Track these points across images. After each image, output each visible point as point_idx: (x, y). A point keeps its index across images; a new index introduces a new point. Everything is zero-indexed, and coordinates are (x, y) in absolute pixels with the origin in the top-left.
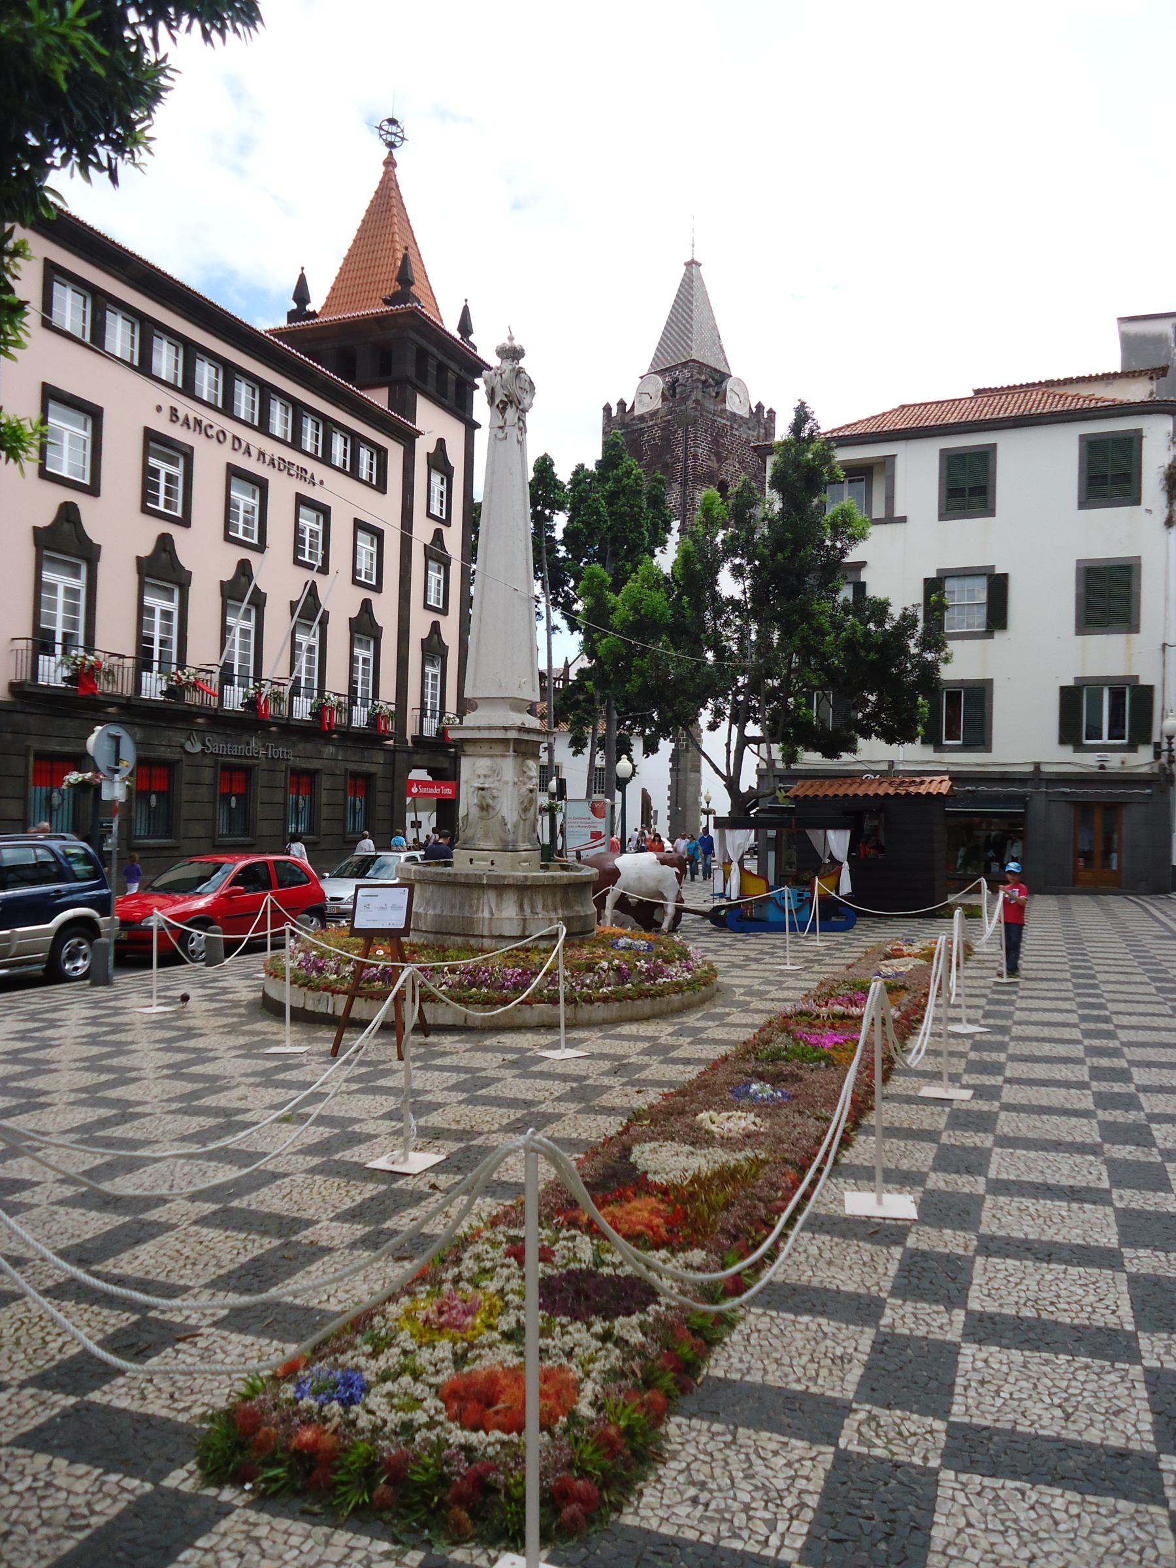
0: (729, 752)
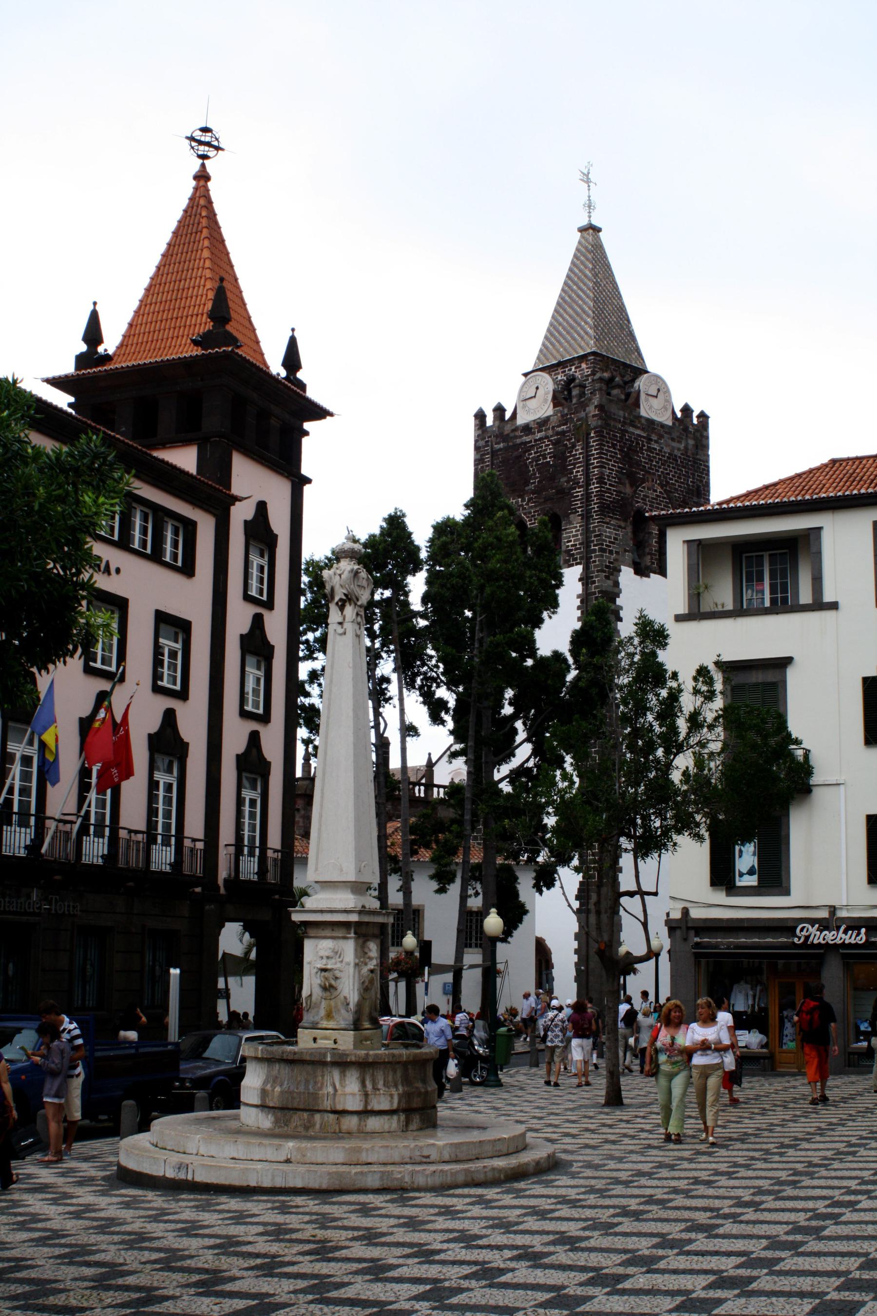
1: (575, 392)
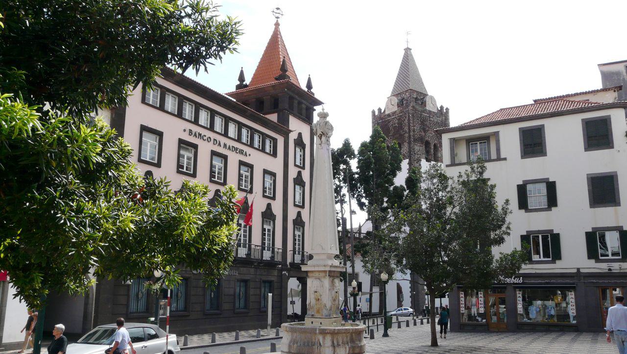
1: (404, 102)
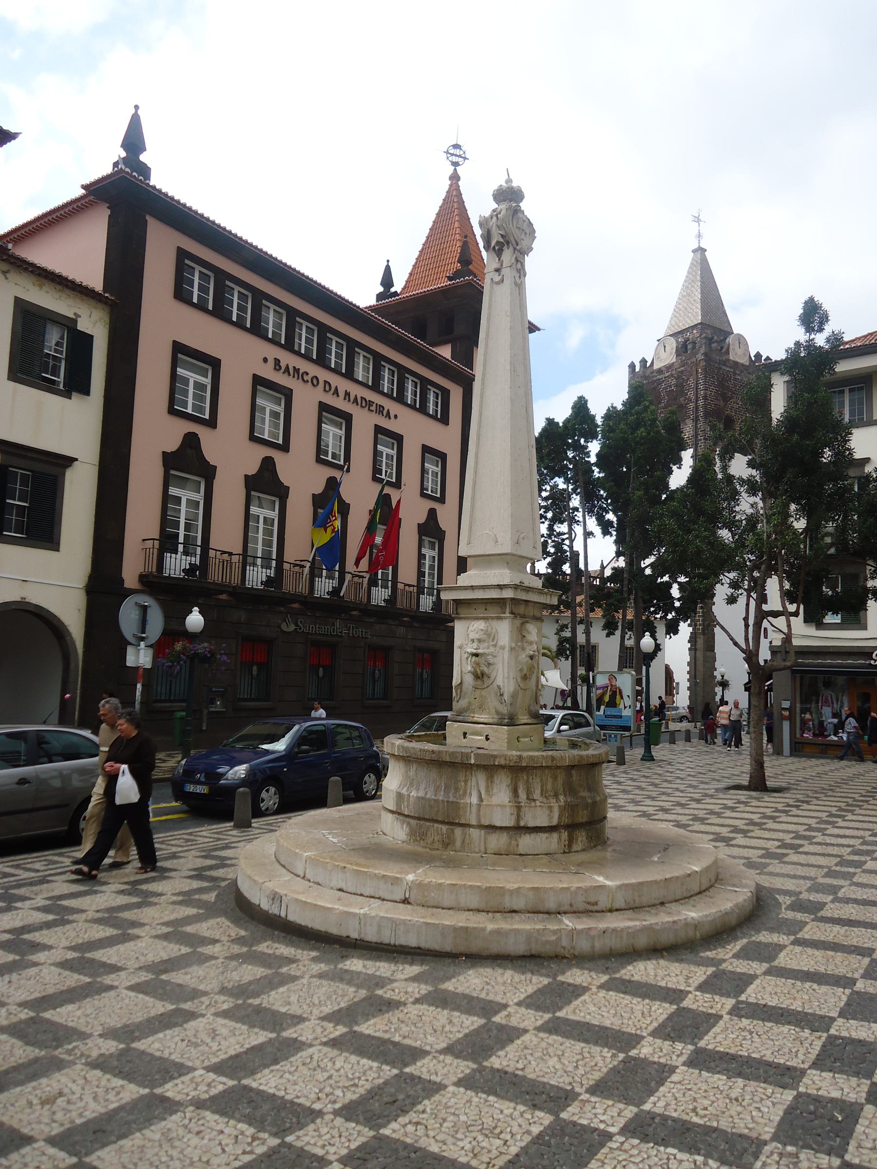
0: (747, 626)
1: (690, 347)
